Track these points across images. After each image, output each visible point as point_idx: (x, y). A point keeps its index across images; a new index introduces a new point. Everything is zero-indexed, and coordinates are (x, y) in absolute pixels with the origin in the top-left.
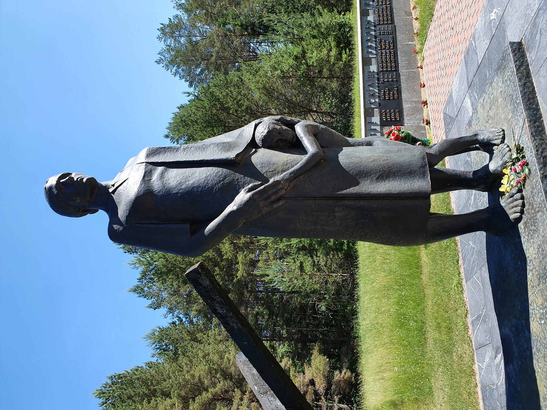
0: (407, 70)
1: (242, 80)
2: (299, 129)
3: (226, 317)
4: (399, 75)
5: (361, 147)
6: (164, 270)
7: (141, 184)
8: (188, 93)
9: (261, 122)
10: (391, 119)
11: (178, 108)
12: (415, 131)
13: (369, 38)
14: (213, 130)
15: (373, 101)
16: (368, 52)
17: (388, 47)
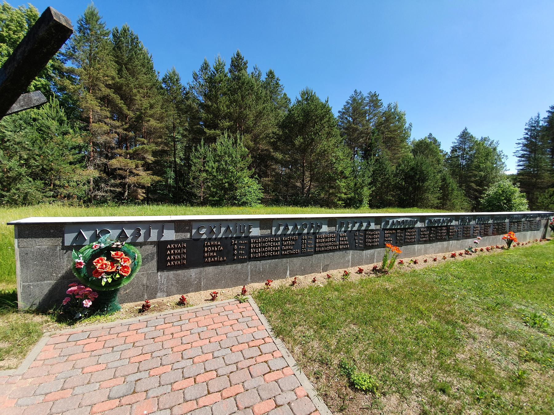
0: (249, 270)
8: (328, 101)
12: (147, 287)
13: (299, 227)
16: (280, 225)
17: (285, 248)
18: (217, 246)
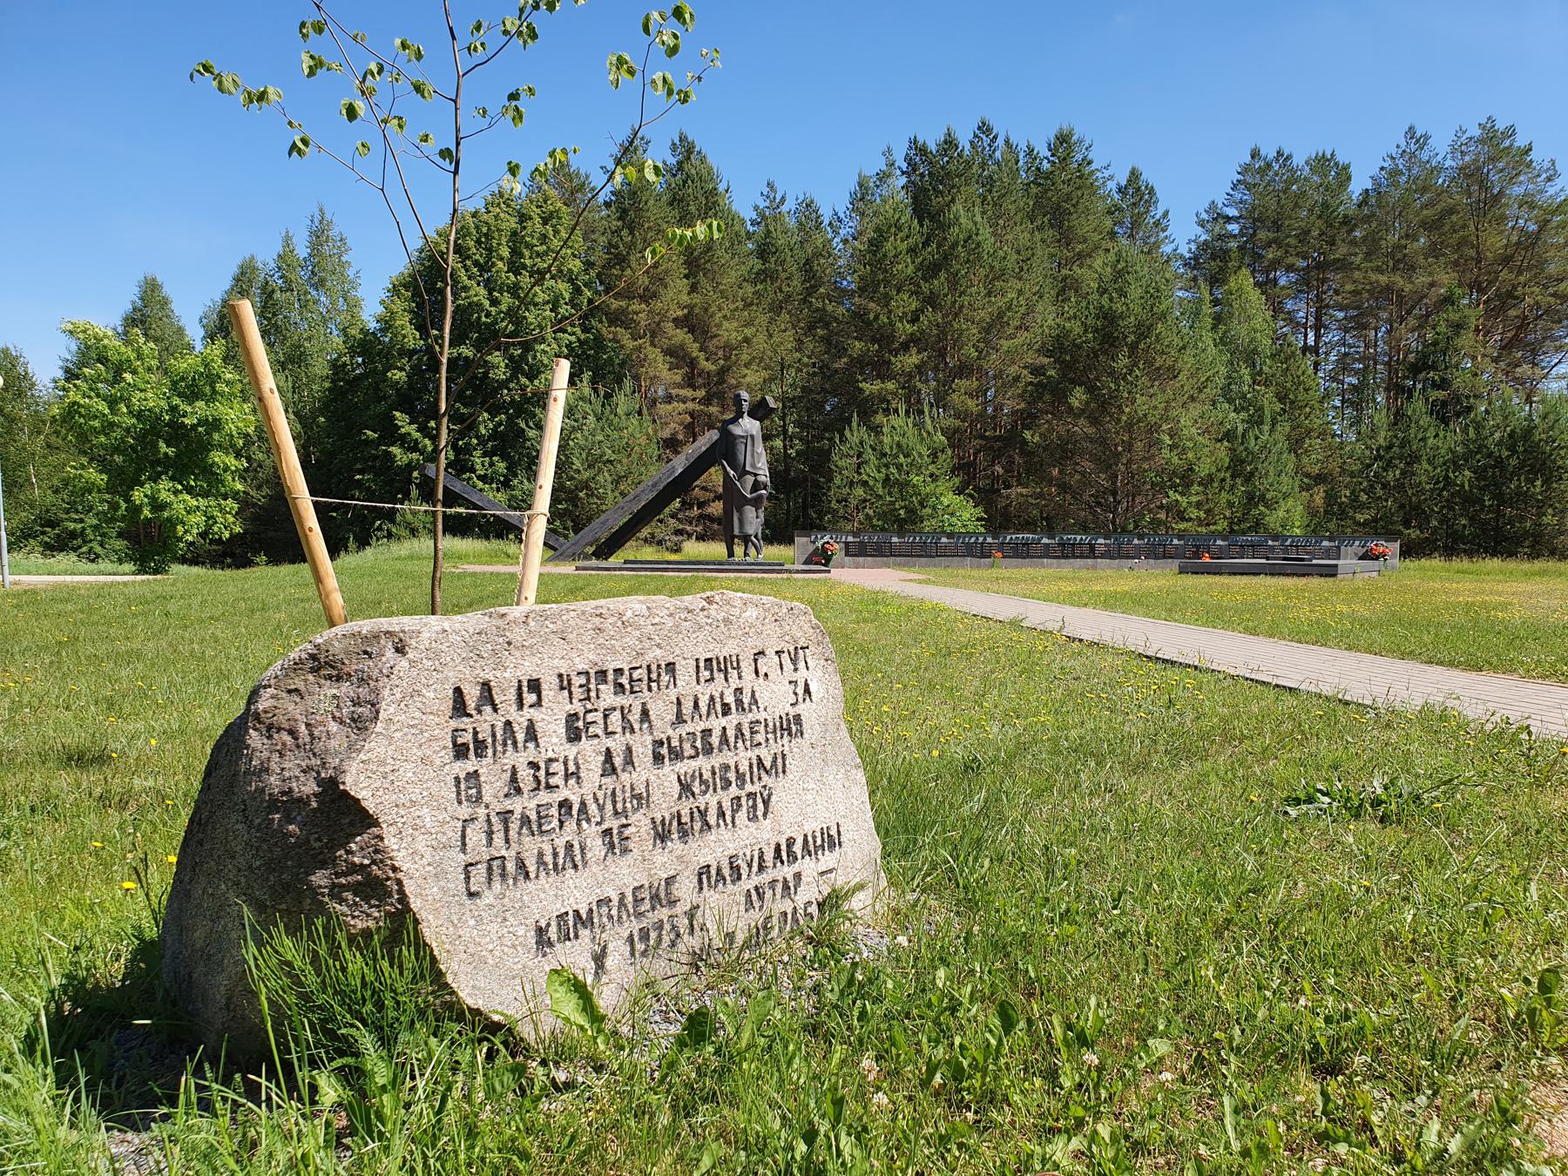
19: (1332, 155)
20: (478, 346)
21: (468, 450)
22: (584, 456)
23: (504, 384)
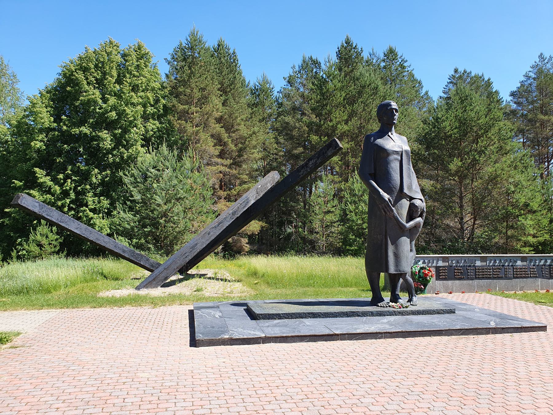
1: (506, 154)
2: (419, 219)
3: (307, 167)
4: (473, 280)
5: (410, 247)
6: (325, 90)
7: (392, 150)
9: (422, 201)
10: (441, 273)
11: (489, 79)
14: (456, 128)
15: (454, 262)
16: (491, 260)
18: (460, 270)
19: (483, 75)
20: (94, 127)
21: (83, 193)
22: (164, 194)
23: (110, 152)
